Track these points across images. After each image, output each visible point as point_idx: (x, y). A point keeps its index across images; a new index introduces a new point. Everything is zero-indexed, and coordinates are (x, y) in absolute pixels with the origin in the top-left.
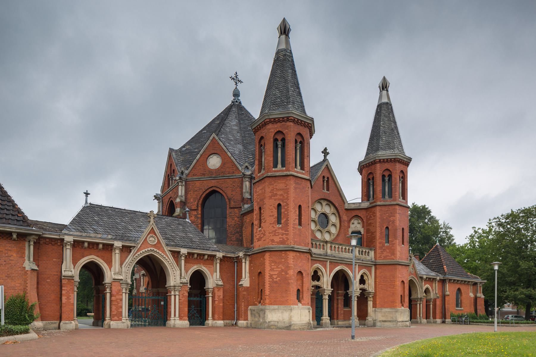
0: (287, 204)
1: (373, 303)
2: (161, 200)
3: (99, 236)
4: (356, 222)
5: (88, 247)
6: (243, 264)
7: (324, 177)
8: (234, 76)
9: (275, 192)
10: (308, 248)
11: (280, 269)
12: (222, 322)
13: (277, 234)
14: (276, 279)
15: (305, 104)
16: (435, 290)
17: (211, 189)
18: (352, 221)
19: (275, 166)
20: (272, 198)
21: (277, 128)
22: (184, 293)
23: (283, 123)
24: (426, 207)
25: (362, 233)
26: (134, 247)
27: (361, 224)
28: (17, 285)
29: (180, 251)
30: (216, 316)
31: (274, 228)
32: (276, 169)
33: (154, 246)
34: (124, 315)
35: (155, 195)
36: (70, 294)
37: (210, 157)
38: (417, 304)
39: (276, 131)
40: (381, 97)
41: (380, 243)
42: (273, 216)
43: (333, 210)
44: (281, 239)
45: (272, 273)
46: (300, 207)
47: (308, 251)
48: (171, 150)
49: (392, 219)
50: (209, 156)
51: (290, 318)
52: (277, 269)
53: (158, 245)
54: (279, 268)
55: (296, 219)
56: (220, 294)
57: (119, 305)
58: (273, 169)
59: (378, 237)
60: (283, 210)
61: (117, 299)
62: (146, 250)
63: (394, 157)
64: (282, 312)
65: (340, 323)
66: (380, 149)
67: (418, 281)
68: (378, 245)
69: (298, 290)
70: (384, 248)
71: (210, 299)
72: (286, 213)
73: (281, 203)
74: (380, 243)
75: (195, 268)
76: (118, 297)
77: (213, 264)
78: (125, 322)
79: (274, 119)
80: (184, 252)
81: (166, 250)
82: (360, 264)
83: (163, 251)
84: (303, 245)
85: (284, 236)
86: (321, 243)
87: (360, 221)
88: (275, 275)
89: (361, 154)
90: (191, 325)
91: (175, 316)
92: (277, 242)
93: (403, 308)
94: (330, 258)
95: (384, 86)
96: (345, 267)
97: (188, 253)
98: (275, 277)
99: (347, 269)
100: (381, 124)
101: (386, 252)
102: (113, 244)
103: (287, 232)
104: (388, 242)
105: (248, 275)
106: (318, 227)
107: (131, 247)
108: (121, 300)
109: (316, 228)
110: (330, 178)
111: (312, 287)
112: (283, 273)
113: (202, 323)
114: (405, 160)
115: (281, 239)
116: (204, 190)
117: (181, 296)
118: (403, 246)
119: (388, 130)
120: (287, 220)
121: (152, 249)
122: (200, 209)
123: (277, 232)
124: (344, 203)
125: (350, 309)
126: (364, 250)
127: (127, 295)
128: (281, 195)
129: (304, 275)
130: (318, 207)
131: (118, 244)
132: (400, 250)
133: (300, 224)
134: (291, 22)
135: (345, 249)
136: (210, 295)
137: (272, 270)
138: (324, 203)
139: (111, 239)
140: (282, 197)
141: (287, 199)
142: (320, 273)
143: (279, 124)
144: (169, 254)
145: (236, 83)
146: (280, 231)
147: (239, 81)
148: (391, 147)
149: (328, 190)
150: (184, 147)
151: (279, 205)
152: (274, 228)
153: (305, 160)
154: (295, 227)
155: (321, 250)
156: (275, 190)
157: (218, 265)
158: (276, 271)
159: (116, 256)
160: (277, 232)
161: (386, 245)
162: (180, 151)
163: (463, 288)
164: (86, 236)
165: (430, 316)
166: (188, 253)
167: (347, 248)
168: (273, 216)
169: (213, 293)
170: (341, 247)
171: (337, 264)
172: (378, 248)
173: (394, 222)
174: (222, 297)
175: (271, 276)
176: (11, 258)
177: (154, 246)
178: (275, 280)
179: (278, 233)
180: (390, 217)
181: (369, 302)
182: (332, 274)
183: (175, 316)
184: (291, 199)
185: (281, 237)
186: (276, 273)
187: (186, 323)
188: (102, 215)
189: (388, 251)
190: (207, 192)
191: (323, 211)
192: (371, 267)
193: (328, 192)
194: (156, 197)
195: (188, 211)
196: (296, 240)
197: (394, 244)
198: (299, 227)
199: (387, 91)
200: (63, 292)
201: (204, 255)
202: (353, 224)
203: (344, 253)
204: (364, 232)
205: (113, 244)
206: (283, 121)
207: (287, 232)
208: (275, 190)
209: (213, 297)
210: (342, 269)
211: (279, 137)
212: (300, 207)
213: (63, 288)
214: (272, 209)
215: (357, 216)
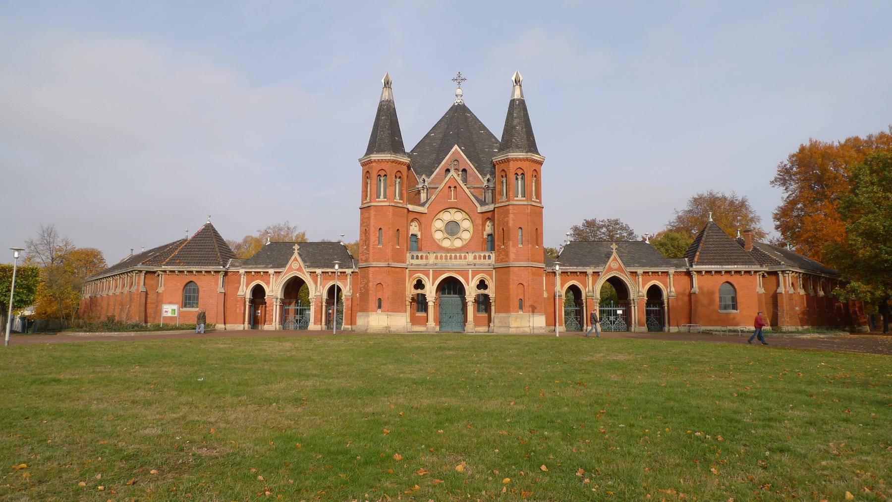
0: (369, 230)
8: (456, 83)
15: (157, 246)
16: (669, 287)
19: (378, 196)
21: (366, 169)
24: (804, 145)
32: (379, 200)
33: (298, 270)
43: (465, 215)
51: (368, 322)
53: (300, 269)
55: (376, 240)
58: (377, 200)
64: (364, 318)
65: (674, 329)
67: (626, 277)
81: (305, 272)
83: (303, 273)
85: (367, 256)
86: (452, 254)
90: (649, 330)
91: (276, 321)
95: (387, 84)
102: (239, 272)
113: (661, 329)
120: (369, 242)
121: (295, 272)
125: (425, 315)
128: (367, 222)
129: (384, 286)
134: (391, 79)
135: (451, 256)
141: (369, 225)
144: (308, 275)
145: (456, 80)
154: (376, 247)
155: (424, 260)
159: (272, 279)
161: (503, 247)
167: (458, 255)
170: (449, 255)
171: (444, 272)
173: (507, 222)
177: (298, 270)
180: (504, 218)
183: (276, 321)
184: (372, 224)
187: (644, 329)
193: (456, 200)
197: (508, 246)
199: (520, 86)
203: (453, 260)
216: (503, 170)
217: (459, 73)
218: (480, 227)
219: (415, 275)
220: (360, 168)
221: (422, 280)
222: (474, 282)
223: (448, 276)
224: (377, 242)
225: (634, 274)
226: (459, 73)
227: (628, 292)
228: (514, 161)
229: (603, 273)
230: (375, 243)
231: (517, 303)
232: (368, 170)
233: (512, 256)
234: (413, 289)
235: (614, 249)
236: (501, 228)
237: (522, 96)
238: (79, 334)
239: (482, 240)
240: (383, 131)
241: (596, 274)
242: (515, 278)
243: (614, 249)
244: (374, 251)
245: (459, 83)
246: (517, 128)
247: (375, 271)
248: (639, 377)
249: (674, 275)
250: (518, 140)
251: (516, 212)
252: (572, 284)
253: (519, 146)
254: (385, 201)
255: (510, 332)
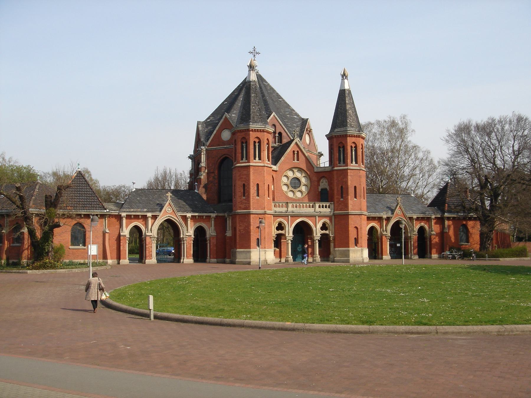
1: (381, 242)
2: (193, 160)
3: (139, 210)
4: (324, 181)
5: (134, 217)
6: (228, 221)
7: (294, 151)
8: (252, 50)
9: (241, 177)
10: (264, 211)
11: (244, 226)
12: (215, 260)
13: (243, 203)
14: (242, 232)
17: (224, 156)
18: (321, 181)
20: (240, 180)
22: (189, 242)
23: (246, 132)
25: (328, 189)
26: (159, 215)
27: (328, 182)
28: (100, 241)
29: (186, 215)
30: (211, 256)
31: (241, 199)
34: (153, 256)
35: (189, 156)
36: (125, 245)
37: (223, 132)
38: (408, 241)
39: (242, 137)
40: (343, 84)
41: (337, 198)
42: (240, 191)
44: (245, 206)
45: (240, 228)
46: (258, 185)
47: (264, 213)
48: (199, 123)
49: (344, 180)
50: (222, 131)
52: (243, 226)
54: (244, 225)
55: (255, 193)
56: (214, 241)
57: (150, 250)
59: (335, 194)
60: (246, 188)
61: (149, 247)
62: (166, 216)
63: (345, 134)
66: (337, 126)
68: (336, 200)
69: (258, 239)
70: (340, 202)
71: (208, 244)
72: (248, 189)
73: (245, 183)
74: (337, 198)
75: (198, 224)
76: (149, 245)
77: (210, 222)
78: (191, 260)
79: (240, 130)
80: (415, 218)
82: (318, 216)
84: (261, 209)
85: (247, 204)
87: (327, 181)
88: (242, 229)
89: (328, 131)
90: (419, 257)
92: (243, 208)
93: (356, 247)
94: (290, 214)
95: (344, 76)
96: (306, 219)
97: (192, 216)
98: (242, 231)
99: (308, 220)
100: (339, 107)
101: (341, 205)
102: (147, 215)
103: (248, 202)
104: (342, 197)
105: (230, 229)
106: (290, 188)
107: (157, 215)
108: (152, 247)
109: (288, 189)
110: (299, 151)
111: (276, 235)
112: (247, 228)
114: (355, 134)
115: (245, 206)
116: (219, 157)
117: (187, 244)
118: (355, 199)
119: (343, 111)
122: (216, 172)
123: (243, 202)
124: (314, 168)
126: (324, 205)
127: (155, 244)
128: (245, 178)
130: (290, 174)
131: (149, 215)
132: (352, 203)
133: (258, 195)
134: (348, 72)
136: (208, 242)
137: (240, 226)
138: (295, 170)
139: (146, 211)
140: (245, 179)
142: (283, 225)
143: (243, 133)
146: (244, 201)
147: (257, 53)
148: (344, 125)
149: (298, 160)
150: (208, 118)
151: (244, 185)
152: (241, 199)
153: (262, 153)
156: (241, 175)
157: (213, 222)
158: (243, 227)
160: (243, 202)
162: (206, 122)
163: (86, 222)
164: (133, 211)
165: (427, 253)
166: (192, 216)
168: (240, 191)
169: (210, 241)
172: (335, 202)
174: (215, 243)
175: (240, 230)
176: (98, 227)
178: (242, 233)
179: (243, 202)
181: (331, 244)
182: (294, 225)
185: (245, 205)
186: (242, 228)
188: (142, 196)
189: (343, 204)
190: (222, 158)
191: (295, 176)
192: (332, 216)
193: (299, 162)
194: (190, 157)
195: (197, 185)
196: (254, 206)
198: (257, 198)
200: (121, 244)
201: (203, 216)
202: (322, 182)
203: (302, 208)
204: (329, 189)
205: (147, 215)
206: (246, 131)
207: (248, 202)
208: (241, 175)
209: (210, 243)
210: (303, 221)
211: (244, 141)
212: (258, 185)
213: (121, 242)
214: (240, 187)
215: (323, 177)
216: (341, 142)
217: (254, 47)
218: (316, 183)
219: (277, 220)
220: (327, 142)
221: (282, 223)
222: (320, 225)
223: (301, 220)
224: (256, 194)
225: (185, 218)
226: (254, 47)
227: (180, 232)
228: (350, 136)
229: (393, 218)
230: (254, 195)
231: (353, 241)
232: (244, 136)
233: (350, 206)
234: (276, 230)
235: (169, 196)
236: (340, 186)
237: (249, 71)
238: (386, 255)
239: (318, 193)
240: (254, 106)
241: (155, 217)
242: (352, 223)
243: (169, 196)
244: (253, 201)
245: (254, 55)
246: (349, 111)
247: (254, 217)
248: (523, 281)
249: (215, 219)
250: (351, 121)
251: (352, 174)
252: (372, 225)
253: (352, 126)
254: (260, 163)
255: (254, 263)
